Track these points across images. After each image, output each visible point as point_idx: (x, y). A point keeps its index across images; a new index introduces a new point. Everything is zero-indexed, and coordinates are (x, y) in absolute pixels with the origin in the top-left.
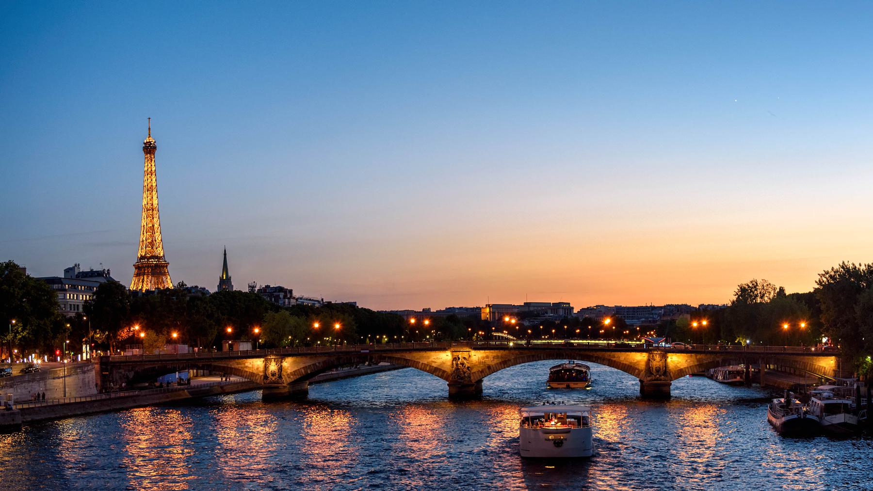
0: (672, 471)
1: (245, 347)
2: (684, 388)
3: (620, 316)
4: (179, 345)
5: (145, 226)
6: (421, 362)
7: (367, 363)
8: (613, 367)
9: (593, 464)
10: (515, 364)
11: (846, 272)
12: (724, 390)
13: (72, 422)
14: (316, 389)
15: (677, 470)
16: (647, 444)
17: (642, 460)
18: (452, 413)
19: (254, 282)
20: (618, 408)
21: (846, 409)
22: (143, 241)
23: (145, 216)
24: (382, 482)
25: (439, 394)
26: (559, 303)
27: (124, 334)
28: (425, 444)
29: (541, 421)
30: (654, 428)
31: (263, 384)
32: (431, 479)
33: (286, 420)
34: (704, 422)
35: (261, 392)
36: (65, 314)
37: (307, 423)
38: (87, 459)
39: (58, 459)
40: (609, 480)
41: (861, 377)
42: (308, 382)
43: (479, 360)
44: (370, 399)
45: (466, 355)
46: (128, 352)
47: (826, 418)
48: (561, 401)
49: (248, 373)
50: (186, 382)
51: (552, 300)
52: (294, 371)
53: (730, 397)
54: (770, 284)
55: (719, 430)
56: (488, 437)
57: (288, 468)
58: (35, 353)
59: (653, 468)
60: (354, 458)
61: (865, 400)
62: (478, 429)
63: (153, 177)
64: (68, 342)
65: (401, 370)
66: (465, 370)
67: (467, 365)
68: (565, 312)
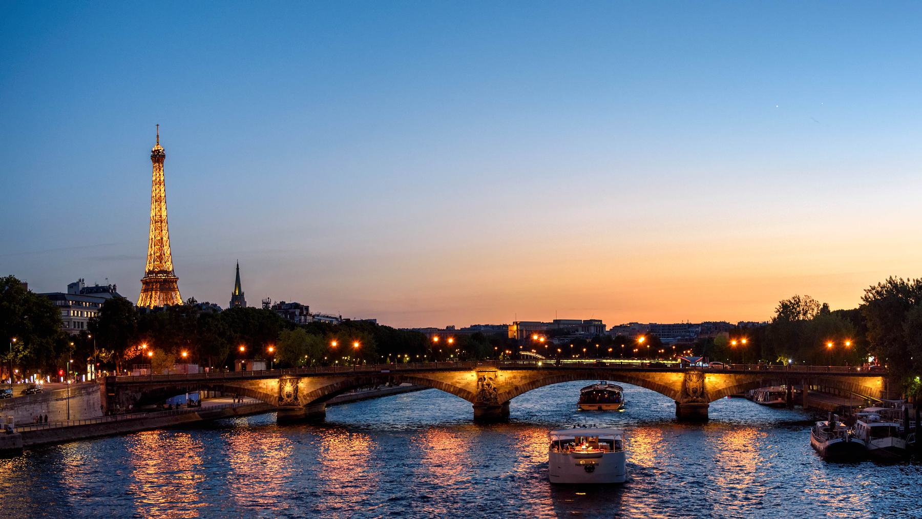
0: (709, 498)
1: (259, 366)
2: (723, 410)
3: (655, 334)
4: (189, 365)
5: (154, 239)
6: (445, 383)
7: (388, 384)
8: (647, 388)
9: (626, 490)
10: (544, 385)
11: (894, 287)
12: (764, 412)
13: (77, 446)
14: (334, 411)
15: (714, 497)
16: (683, 469)
17: (678, 486)
18: (478, 437)
19: (268, 298)
20: (652, 431)
21: (893, 432)
22: (151, 255)
23: (154, 229)
24: (403, 509)
25: (463, 416)
26: (591, 320)
27: (131, 353)
28: (449, 469)
29: (571, 445)
30: (690, 452)
31: (277, 406)
32: (455, 506)
33: (302, 443)
34: (744, 446)
35: (276, 414)
36: (68, 332)
37: (324, 447)
38: (92, 485)
39: (61, 485)
40: (643, 508)
41: (909, 399)
42: (325, 404)
43: (506, 380)
44: (391, 422)
45: (492, 375)
46: (136, 372)
47: (872, 442)
48: (593, 424)
49: (262, 394)
50: (197, 404)
51: (584, 317)
52: (310, 393)
53: (771, 420)
54: (813, 300)
55: (760, 455)
56: (515, 462)
57: (304, 494)
58: (37, 373)
59: (690, 495)
60: (374, 484)
61: (914, 423)
62: (505, 454)
63: (161, 188)
64: (72, 361)
65: (424, 391)
66: (491, 391)
67: (493, 386)
68: (597, 329)
